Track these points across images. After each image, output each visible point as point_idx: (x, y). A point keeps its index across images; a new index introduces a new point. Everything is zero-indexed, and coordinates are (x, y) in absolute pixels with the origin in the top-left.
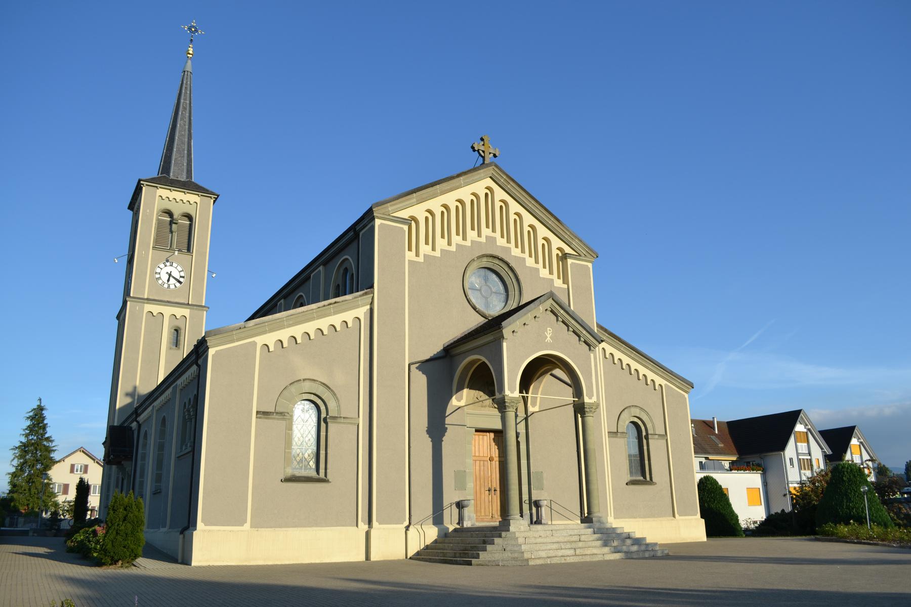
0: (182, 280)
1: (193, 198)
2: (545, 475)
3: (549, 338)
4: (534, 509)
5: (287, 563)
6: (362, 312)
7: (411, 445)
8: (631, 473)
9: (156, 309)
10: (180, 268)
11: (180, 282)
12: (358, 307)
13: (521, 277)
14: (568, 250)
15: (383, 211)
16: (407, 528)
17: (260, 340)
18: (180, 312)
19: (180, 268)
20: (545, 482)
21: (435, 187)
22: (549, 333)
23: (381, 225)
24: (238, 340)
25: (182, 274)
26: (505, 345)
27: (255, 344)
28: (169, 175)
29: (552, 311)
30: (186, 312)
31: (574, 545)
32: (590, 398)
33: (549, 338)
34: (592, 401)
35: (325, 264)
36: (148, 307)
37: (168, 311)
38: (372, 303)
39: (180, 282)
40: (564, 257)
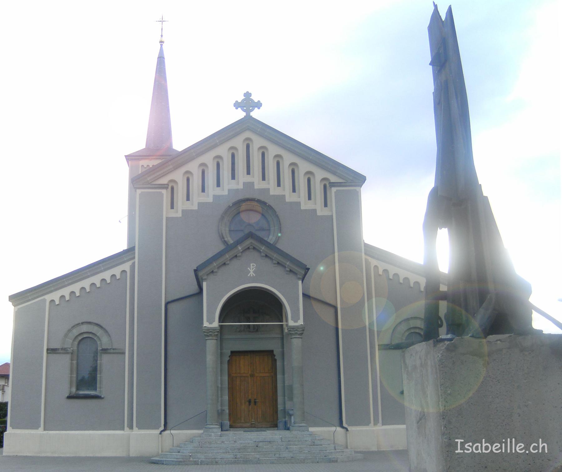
22: (252, 270)
27: (45, 300)
32: (296, 321)
40: (327, 186)
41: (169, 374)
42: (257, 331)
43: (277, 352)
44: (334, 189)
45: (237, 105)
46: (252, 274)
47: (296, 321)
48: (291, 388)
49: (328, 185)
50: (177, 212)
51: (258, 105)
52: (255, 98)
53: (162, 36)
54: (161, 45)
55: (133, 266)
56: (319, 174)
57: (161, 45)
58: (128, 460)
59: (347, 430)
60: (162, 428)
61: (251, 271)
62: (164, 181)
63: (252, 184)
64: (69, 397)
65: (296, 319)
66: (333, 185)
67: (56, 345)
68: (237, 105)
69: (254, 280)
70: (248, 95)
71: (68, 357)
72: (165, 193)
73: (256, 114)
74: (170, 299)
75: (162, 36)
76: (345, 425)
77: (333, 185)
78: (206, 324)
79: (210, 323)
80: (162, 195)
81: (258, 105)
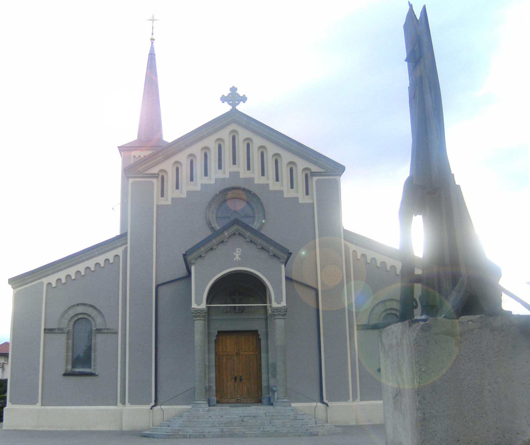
22: (237, 255)
27: (42, 283)
32: (279, 303)
40: (308, 175)
41: (159, 353)
42: (242, 312)
43: (261, 332)
44: (315, 179)
45: (224, 99)
46: (237, 258)
47: (279, 303)
48: (274, 366)
49: (309, 175)
50: (167, 200)
51: (244, 99)
52: (241, 92)
53: (153, 34)
54: (152, 43)
55: (125, 251)
56: (301, 164)
57: (152, 43)
58: (121, 434)
59: (327, 405)
60: (153, 403)
61: (237, 255)
62: (155, 170)
63: (238, 173)
64: (66, 375)
65: (279, 301)
66: (314, 174)
67: (53, 325)
68: (224, 99)
69: (239, 264)
70: (233, 90)
71: (64, 336)
72: (156, 182)
73: (241, 107)
74: (160, 282)
75: (153, 34)
76: (325, 400)
77: (314, 174)
78: (194, 306)
79: (199, 305)
80: (153, 184)
81: (244, 99)
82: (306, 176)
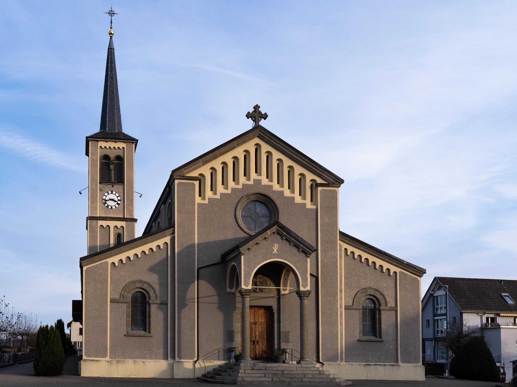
0: (119, 202)
1: (121, 145)
2: (291, 334)
3: (275, 251)
4: (210, 354)
5: (133, 377)
6: (168, 239)
7: (199, 315)
8: (364, 333)
9: (105, 223)
10: (117, 195)
11: (118, 204)
12: (166, 236)
13: (234, 220)
14: (319, 181)
15: (179, 174)
16: (196, 362)
17: (110, 260)
18: (119, 224)
19: (117, 195)
20: (291, 338)
21: (215, 152)
22: (276, 248)
23: (179, 184)
24: (98, 261)
25: (119, 198)
26: (242, 257)
27: (107, 262)
28: (106, 130)
29: (278, 234)
30: (123, 223)
31: (246, 375)
32: (305, 288)
33: (275, 251)
34: (305, 290)
35: (164, 203)
36: (100, 223)
37: (112, 224)
38: (174, 233)
39: (118, 204)
40: (315, 185)
41: (200, 321)
42: (262, 292)
43: (275, 308)
44: (320, 189)
45: (248, 116)
46: (275, 251)
47: (305, 288)
48: (287, 334)
49: (314, 185)
50: (205, 200)
51: (265, 116)
52: (263, 110)
53: (111, 28)
54: (111, 37)
55: (173, 240)
56: (310, 176)
57: (111, 37)
58: (346, 385)
59: (323, 364)
60: (196, 359)
61: (275, 250)
62: (195, 174)
63: (260, 181)
64: (125, 335)
65: (305, 286)
66: (318, 185)
67: (117, 296)
68: (248, 116)
69: (277, 256)
70: (257, 107)
71: (125, 306)
72: (197, 183)
73: (263, 123)
74: (200, 266)
75: (111, 28)
76: (321, 361)
77: (318, 185)
78: (243, 287)
79: (246, 286)
80: (194, 185)
81: (265, 116)
82: (312, 185)
